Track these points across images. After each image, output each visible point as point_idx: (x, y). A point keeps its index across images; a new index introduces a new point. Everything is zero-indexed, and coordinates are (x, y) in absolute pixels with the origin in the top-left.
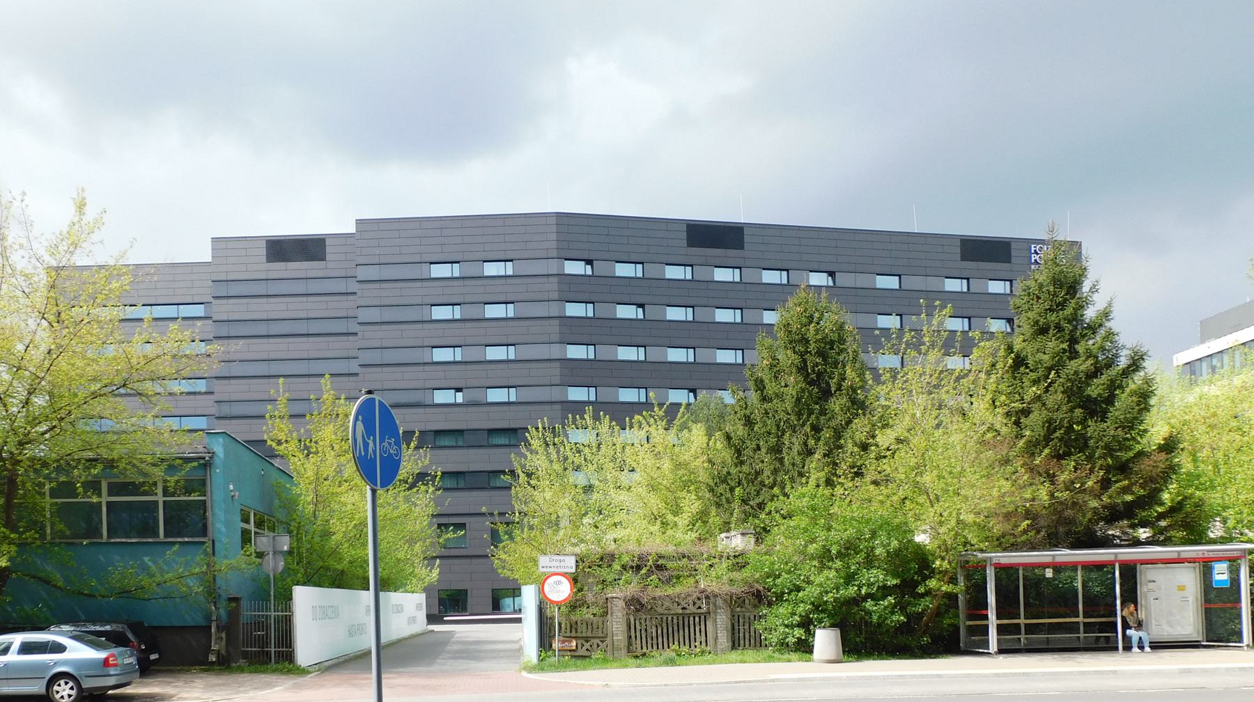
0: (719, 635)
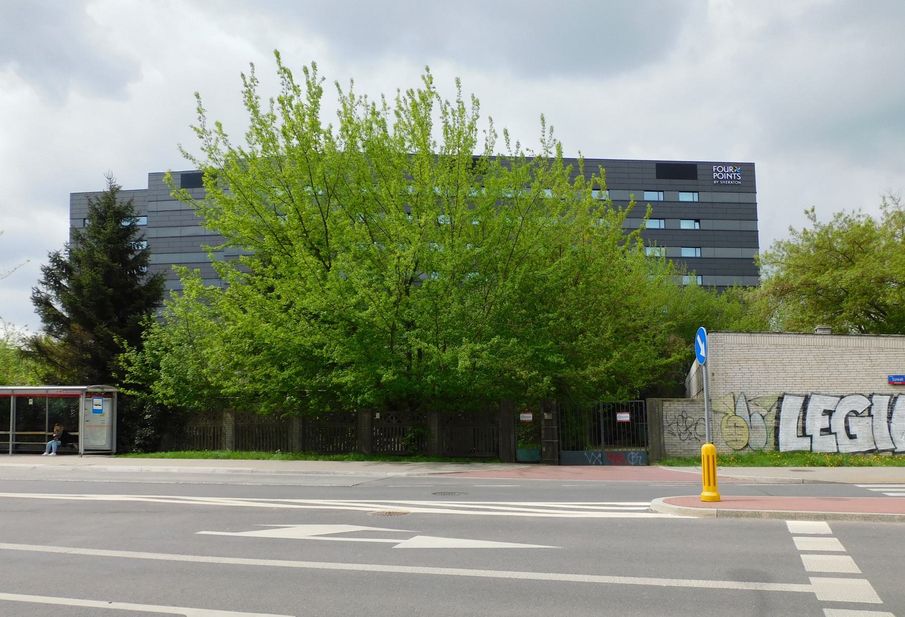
0: (862, 444)
